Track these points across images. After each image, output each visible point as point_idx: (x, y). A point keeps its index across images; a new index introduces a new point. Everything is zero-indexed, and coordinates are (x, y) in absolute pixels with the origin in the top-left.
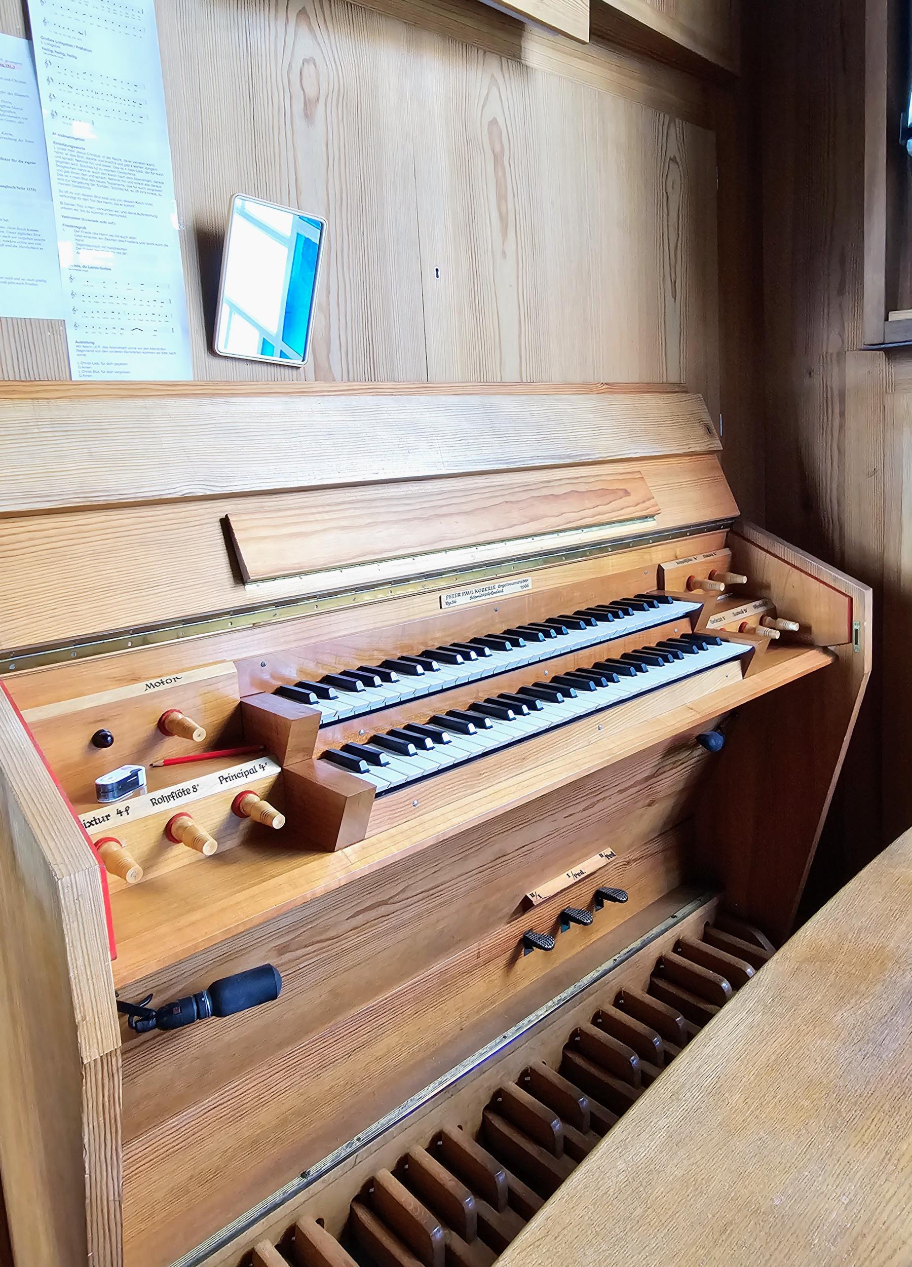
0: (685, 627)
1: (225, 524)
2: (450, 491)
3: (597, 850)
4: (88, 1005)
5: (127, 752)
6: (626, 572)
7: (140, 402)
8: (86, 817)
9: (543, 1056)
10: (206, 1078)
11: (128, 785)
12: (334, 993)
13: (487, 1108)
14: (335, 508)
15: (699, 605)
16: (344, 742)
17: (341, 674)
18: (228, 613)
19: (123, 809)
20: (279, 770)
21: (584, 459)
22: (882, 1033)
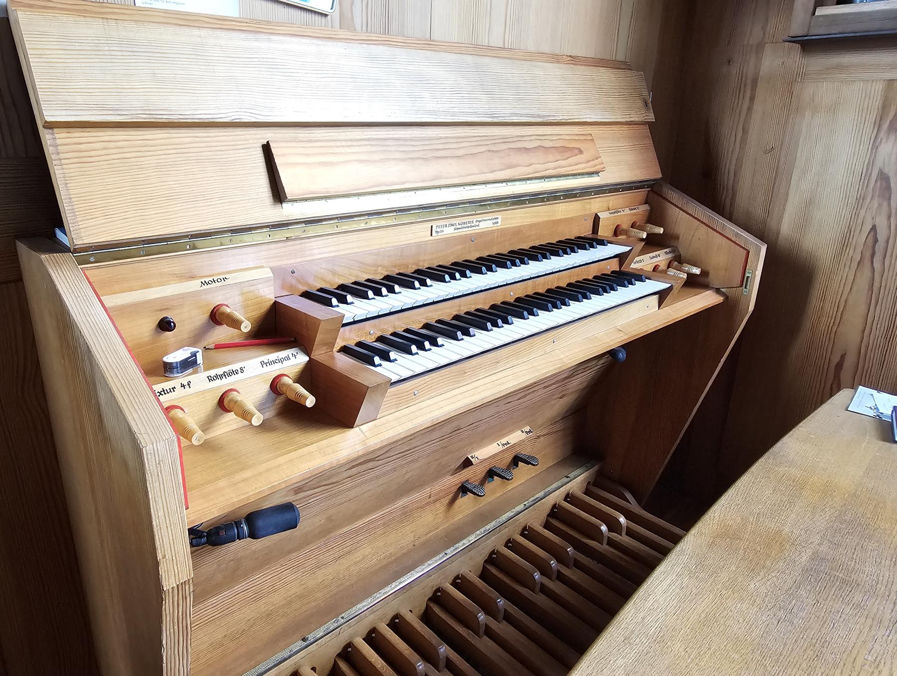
0: (614, 266)
1: (267, 150)
2: (446, 138)
3: (520, 428)
4: (167, 547)
5: (186, 336)
6: (570, 217)
7: (196, 32)
8: (158, 388)
9: (470, 568)
10: (236, 573)
11: (189, 364)
12: (329, 519)
13: (430, 599)
14: (355, 143)
15: (630, 248)
16: (358, 340)
17: (353, 283)
18: (337, 218)
19: (185, 383)
20: (307, 359)
21: (551, 119)
22: (790, 602)
